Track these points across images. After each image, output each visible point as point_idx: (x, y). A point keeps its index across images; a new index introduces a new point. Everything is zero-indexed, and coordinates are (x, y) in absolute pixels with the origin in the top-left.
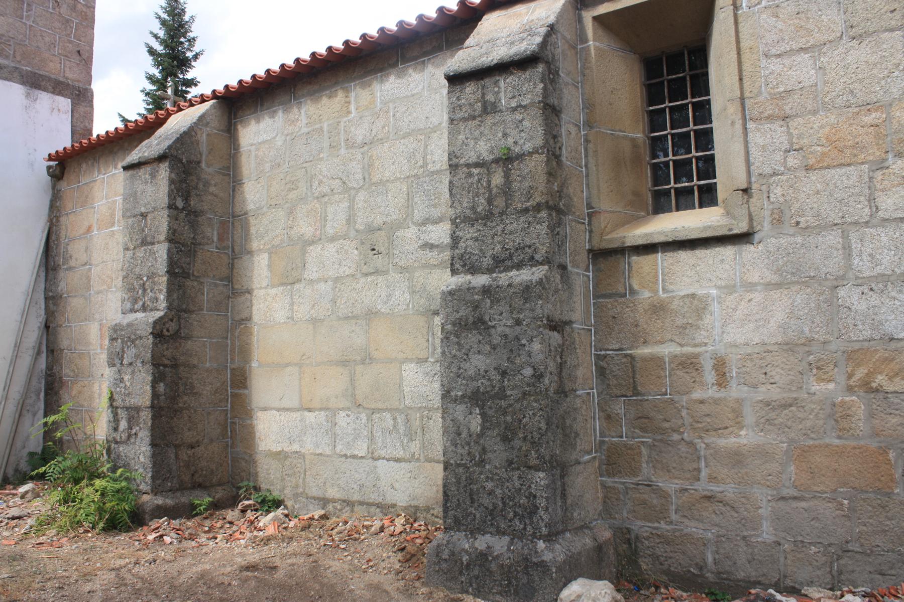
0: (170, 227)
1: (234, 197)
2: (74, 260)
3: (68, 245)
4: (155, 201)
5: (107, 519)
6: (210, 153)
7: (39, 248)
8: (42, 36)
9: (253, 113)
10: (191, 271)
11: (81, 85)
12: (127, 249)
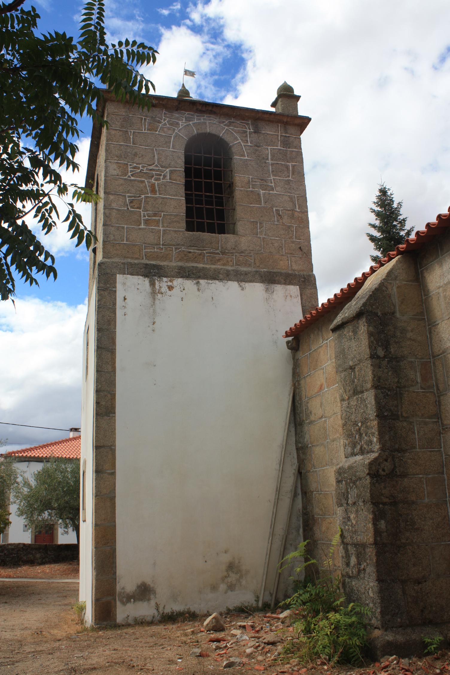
0: (374, 375)
1: (431, 338)
2: (313, 415)
3: (308, 403)
4: (359, 354)
5: (341, 653)
6: (402, 303)
7: (288, 408)
8: (272, 243)
9: (435, 259)
10: (400, 413)
11: (305, 273)
12: (343, 400)
